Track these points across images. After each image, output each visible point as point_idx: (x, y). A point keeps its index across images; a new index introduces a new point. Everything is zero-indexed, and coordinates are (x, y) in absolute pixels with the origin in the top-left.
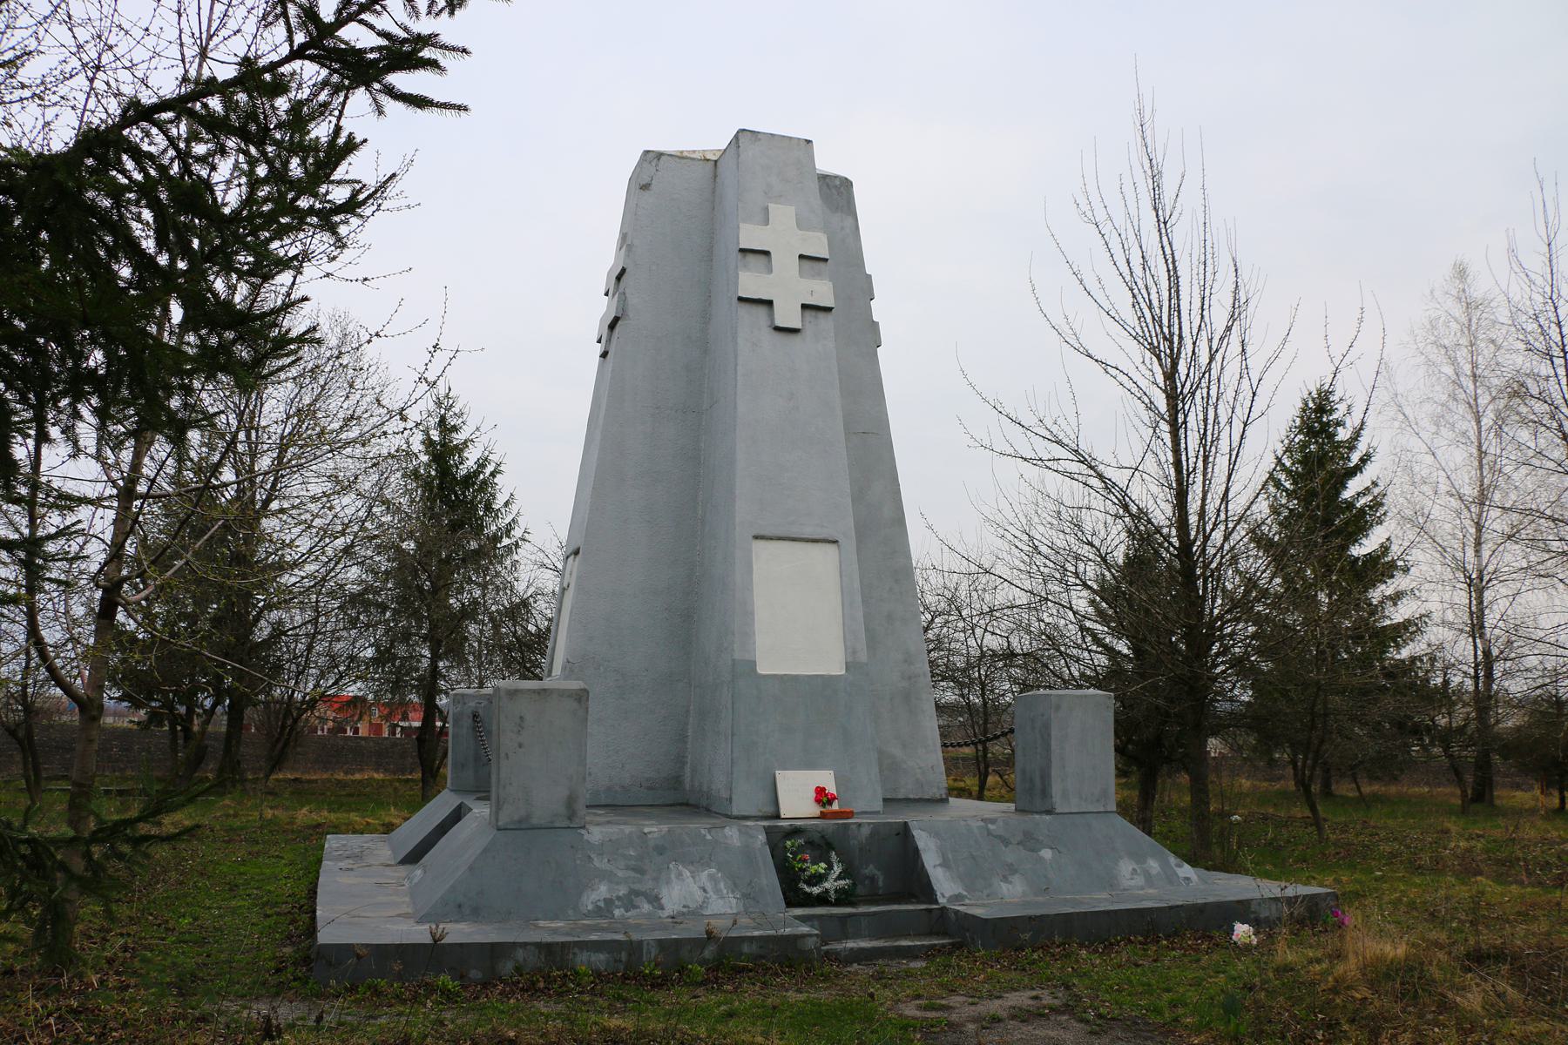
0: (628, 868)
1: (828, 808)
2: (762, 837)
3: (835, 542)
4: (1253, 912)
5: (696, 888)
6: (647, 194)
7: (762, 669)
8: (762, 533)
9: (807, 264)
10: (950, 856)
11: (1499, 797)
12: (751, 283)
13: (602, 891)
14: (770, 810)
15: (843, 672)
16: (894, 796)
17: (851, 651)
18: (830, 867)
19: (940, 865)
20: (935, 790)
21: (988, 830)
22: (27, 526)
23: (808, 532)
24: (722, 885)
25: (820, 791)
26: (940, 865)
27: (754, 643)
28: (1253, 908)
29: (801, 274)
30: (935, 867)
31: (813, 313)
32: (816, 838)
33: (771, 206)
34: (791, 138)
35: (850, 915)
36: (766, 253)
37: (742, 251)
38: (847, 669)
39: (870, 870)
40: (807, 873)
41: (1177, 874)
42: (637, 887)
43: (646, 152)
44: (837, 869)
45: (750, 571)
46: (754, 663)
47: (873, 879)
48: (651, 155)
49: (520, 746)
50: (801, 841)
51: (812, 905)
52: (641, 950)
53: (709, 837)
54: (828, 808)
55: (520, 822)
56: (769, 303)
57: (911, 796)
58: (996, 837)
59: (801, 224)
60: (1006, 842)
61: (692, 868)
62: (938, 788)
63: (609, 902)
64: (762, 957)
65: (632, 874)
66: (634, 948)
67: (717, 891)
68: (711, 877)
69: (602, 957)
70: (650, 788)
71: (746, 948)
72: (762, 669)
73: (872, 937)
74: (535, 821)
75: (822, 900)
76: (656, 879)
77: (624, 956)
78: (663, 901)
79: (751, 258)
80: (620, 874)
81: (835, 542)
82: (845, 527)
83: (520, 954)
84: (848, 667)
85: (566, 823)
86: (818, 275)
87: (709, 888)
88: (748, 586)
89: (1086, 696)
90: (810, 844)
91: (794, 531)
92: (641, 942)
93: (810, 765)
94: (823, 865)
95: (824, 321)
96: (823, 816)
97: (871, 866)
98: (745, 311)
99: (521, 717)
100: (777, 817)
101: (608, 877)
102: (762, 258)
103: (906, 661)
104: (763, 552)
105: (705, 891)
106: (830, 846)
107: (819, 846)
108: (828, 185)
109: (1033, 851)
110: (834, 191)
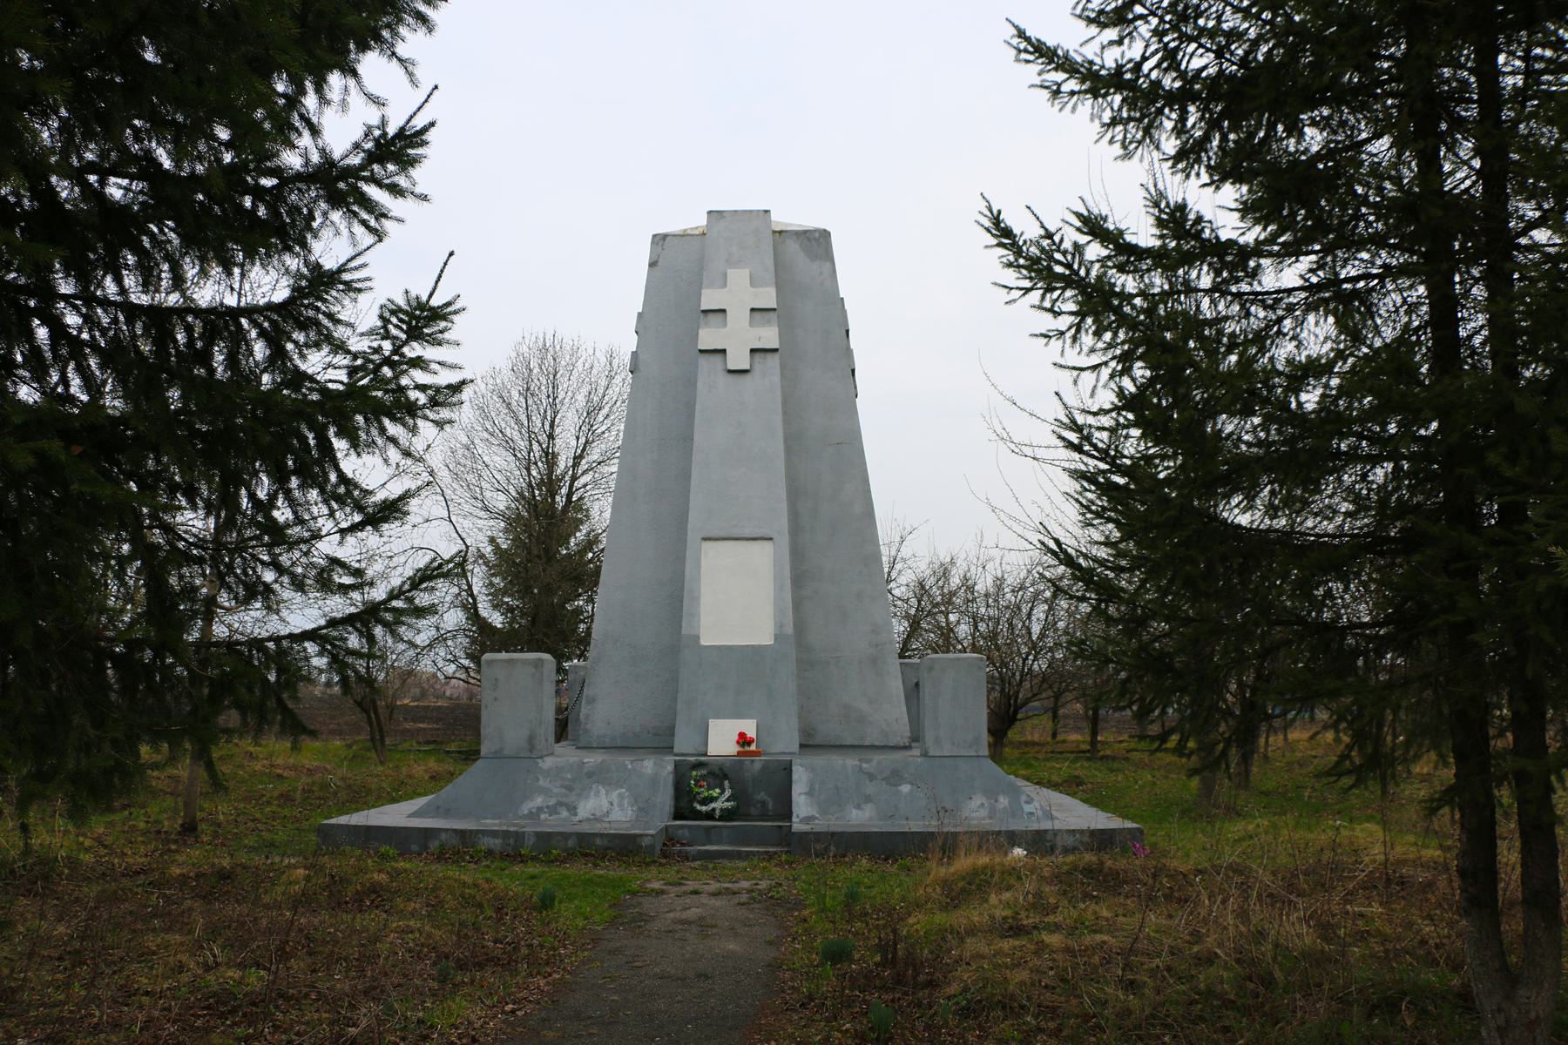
0: (562, 786)
1: (747, 748)
2: (670, 768)
3: (771, 539)
4: (1048, 841)
5: (606, 801)
6: (655, 269)
7: (704, 642)
8: (710, 535)
9: (757, 315)
10: (817, 787)
11: (1104, 743)
12: (708, 337)
13: (539, 801)
14: (701, 749)
15: (772, 642)
16: (861, 743)
17: (779, 626)
18: (723, 791)
19: (806, 793)
20: (899, 739)
21: (861, 768)
23: (747, 533)
24: (626, 801)
25: (742, 735)
26: (806, 793)
27: (699, 621)
28: (1048, 837)
29: (751, 324)
30: (800, 794)
31: (762, 355)
32: (716, 770)
33: (729, 271)
34: (751, 211)
35: (714, 827)
36: (724, 311)
37: (704, 311)
38: (776, 639)
39: (762, 796)
40: (702, 796)
41: (1022, 809)
42: (564, 800)
43: (654, 236)
44: (728, 793)
45: (699, 567)
46: (698, 637)
47: (764, 803)
48: (658, 237)
49: (496, 699)
50: (704, 772)
51: (701, 819)
52: (524, 839)
53: (630, 767)
54: (747, 748)
55: (496, 752)
56: (724, 351)
57: (877, 744)
58: (865, 773)
59: (753, 282)
60: (872, 777)
61: (607, 788)
62: (902, 737)
63: (540, 810)
64: (609, 848)
65: (563, 790)
66: (519, 836)
67: (621, 805)
68: (621, 796)
69: (498, 841)
70: (656, 735)
71: (598, 841)
72: (704, 642)
73: (730, 844)
74: (506, 752)
75: (709, 816)
76: (579, 795)
77: (512, 841)
78: (578, 810)
79: (711, 316)
80: (555, 790)
81: (771, 539)
82: (780, 525)
83: (443, 836)
84: (777, 637)
85: (528, 754)
86: (769, 323)
87: (615, 804)
88: (697, 578)
89: (958, 659)
90: (711, 774)
91: (736, 532)
92: (524, 833)
93: (738, 715)
94: (718, 790)
95: (773, 360)
96: (739, 754)
97: (762, 794)
98: (704, 361)
99: (496, 679)
100: (706, 755)
101: (546, 792)
102: (720, 315)
103: (873, 631)
104: (707, 545)
105: (612, 804)
106: (726, 777)
107: (718, 776)
108: (808, 239)
109: (894, 785)
110: (814, 243)
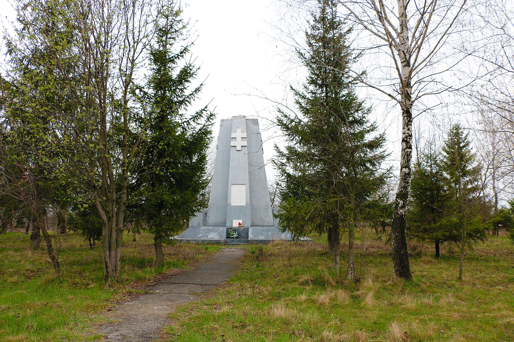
12: (233, 143)
17: (247, 202)
22: (370, 165)
25: (239, 223)
75: (233, 238)
101: (202, 233)
104: (233, 187)
106: (236, 231)
